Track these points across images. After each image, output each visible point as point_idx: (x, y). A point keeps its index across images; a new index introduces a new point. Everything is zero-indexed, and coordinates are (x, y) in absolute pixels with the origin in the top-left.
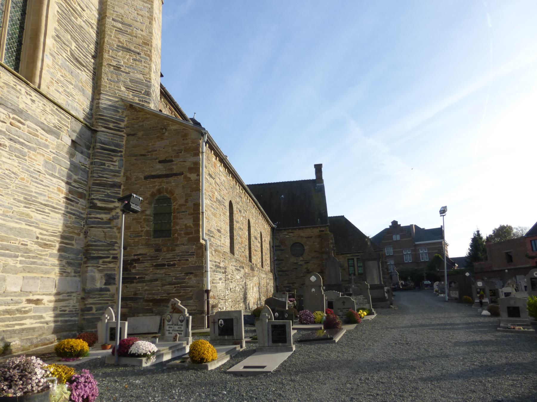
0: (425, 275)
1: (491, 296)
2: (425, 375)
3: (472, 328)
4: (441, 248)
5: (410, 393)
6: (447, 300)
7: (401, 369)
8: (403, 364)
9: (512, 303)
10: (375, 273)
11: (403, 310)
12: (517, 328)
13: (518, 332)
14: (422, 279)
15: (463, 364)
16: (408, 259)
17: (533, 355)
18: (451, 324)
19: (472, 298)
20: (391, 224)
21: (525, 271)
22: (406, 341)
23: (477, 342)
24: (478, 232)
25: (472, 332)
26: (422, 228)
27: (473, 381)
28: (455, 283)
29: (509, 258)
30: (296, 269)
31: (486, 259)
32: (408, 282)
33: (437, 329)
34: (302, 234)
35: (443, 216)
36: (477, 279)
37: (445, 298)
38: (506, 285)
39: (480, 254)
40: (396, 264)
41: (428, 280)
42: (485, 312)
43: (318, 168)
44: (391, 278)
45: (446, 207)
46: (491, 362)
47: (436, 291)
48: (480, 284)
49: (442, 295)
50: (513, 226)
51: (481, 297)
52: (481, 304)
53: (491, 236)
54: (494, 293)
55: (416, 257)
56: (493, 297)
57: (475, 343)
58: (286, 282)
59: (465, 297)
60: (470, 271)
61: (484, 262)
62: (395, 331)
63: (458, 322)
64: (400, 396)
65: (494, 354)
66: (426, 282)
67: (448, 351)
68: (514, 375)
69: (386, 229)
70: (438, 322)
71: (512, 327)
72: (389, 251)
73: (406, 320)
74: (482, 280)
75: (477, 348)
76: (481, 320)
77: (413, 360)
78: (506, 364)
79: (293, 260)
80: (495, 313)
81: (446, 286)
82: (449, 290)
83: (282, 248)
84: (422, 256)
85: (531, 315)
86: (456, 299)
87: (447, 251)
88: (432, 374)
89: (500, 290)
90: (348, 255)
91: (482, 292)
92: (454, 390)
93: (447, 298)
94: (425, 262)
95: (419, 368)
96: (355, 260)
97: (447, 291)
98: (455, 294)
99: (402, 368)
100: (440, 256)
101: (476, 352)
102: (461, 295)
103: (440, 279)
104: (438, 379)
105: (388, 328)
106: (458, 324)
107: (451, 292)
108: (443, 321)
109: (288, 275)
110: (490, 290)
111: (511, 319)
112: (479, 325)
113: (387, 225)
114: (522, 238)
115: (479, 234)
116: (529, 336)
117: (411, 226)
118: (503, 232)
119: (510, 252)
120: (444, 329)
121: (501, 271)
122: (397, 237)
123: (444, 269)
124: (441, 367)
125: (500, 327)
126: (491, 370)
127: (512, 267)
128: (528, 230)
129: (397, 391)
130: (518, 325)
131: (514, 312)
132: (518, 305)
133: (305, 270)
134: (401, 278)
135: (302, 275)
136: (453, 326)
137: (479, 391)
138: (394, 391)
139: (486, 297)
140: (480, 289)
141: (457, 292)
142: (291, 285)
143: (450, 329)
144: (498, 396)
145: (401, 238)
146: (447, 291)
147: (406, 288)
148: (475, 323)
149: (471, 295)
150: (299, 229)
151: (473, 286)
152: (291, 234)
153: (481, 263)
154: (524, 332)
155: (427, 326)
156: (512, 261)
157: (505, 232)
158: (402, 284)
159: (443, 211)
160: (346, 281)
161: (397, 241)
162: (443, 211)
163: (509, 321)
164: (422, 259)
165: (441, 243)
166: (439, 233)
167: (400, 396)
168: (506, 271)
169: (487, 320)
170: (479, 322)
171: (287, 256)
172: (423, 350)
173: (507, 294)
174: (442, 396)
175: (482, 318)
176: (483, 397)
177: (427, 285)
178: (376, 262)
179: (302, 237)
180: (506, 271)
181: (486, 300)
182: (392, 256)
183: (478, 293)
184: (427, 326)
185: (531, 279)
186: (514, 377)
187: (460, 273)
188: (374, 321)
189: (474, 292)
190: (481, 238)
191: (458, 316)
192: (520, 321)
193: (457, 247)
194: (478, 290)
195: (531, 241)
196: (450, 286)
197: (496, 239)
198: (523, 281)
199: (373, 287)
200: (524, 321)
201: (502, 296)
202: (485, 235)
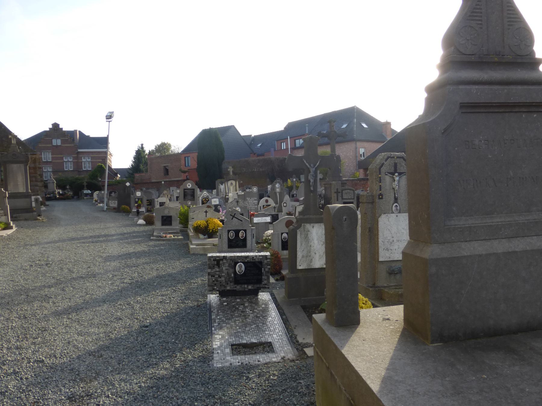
0: (85, 184)
1: (147, 205)
2: (63, 305)
3: (127, 238)
4: (104, 157)
5: (34, 338)
6: (105, 209)
7: (29, 303)
8: (35, 294)
9: (166, 213)
10: (20, 179)
11: (52, 222)
12: (168, 236)
13: (169, 240)
14: (82, 188)
15: (112, 284)
16: (69, 166)
17: (181, 263)
18: (105, 236)
19: (130, 207)
21: (178, 184)
22: (47, 261)
23: (129, 254)
24: (142, 145)
25: (126, 243)
26: (87, 135)
27: (120, 305)
28: (115, 192)
29: (166, 171)
31: (147, 171)
32: (66, 191)
33: (89, 242)
35: (109, 122)
36: (136, 189)
37: (103, 207)
38: (161, 195)
39: (141, 166)
40: (54, 172)
41: (88, 189)
42: (141, 221)
44: (46, 186)
45: (113, 112)
46: (142, 277)
47: (96, 201)
48: (138, 194)
49: (101, 205)
50: (172, 144)
51: (139, 206)
52: (138, 213)
53: (153, 151)
54: (151, 203)
55: (78, 165)
56: (149, 207)
57: (129, 256)
59: (124, 206)
60: (132, 182)
62: (35, 248)
63: (113, 232)
64: (17, 348)
65: (146, 266)
66: (86, 192)
67: (96, 268)
68: (164, 289)
69: (45, 132)
70: (91, 234)
71: (164, 235)
72: (47, 156)
73: (54, 233)
74: (141, 190)
75: (129, 262)
76: (136, 229)
77: (50, 287)
78: (157, 277)
80: (149, 222)
81: (105, 196)
82: (109, 200)
84: (85, 164)
85: (180, 223)
86: (114, 208)
87: (111, 161)
88: (72, 304)
89: (156, 200)
91: (140, 202)
92: (96, 321)
93: (106, 207)
94: (87, 171)
95: (56, 297)
97: (106, 200)
98: (114, 204)
99: (29, 301)
100: (103, 166)
101: (128, 266)
102: (119, 205)
103: (100, 188)
104: (77, 309)
105: (26, 245)
106: (113, 235)
107: (110, 201)
108: (97, 233)
110: (147, 200)
111: (164, 227)
112: (134, 235)
113: (47, 127)
114: (178, 154)
115: (142, 148)
116: (178, 243)
117: (75, 131)
118: (163, 148)
120: (97, 242)
121: (158, 182)
122: (57, 142)
123: (105, 179)
124: (84, 291)
125: (153, 236)
126: (141, 287)
127: (168, 180)
128: (183, 149)
129: (13, 341)
130: (170, 233)
131: (167, 221)
132: (172, 214)
134: (59, 186)
136: (107, 238)
137: (126, 317)
138: (9, 341)
139: (143, 206)
140: (139, 199)
141: (116, 202)
143: (104, 241)
144: (146, 319)
145: (62, 143)
146: (106, 200)
147: (63, 198)
148: (130, 233)
149: (129, 204)
151: (132, 196)
153: (142, 174)
154: (174, 240)
155: (78, 239)
156: (168, 174)
157: (165, 149)
158: (59, 193)
159: (109, 117)
161: (57, 146)
162: (109, 117)
163: (161, 230)
164: (85, 168)
166: (103, 142)
167: (17, 348)
168: (163, 182)
169: (142, 229)
170: (134, 232)
172: (67, 271)
173: (162, 204)
174: (79, 334)
175: (138, 228)
176: (129, 325)
177: (87, 195)
178: (22, 166)
180: (163, 182)
181: (143, 209)
183: (136, 202)
184: (78, 239)
185: (185, 189)
186: (164, 291)
187: (121, 183)
188: (9, 238)
189: (132, 202)
190: (144, 152)
191: (115, 226)
192: (171, 229)
193: (121, 159)
194: (137, 200)
196: (110, 196)
197: (157, 154)
198: (177, 192)
199: (13, 196)
200: (174, 229)
201: (157, 206)
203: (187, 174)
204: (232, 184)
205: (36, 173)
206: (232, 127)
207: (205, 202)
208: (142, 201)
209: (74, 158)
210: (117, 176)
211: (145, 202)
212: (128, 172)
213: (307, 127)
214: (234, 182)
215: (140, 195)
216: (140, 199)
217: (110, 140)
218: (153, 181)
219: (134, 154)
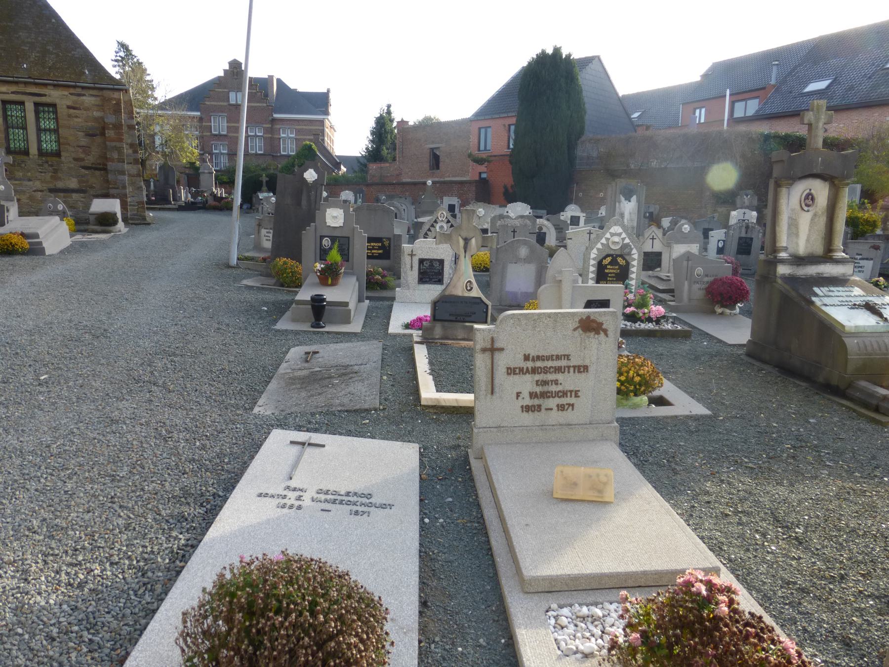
4: (318, 132)
6: (234, 261)
24: (389, 106)
26: (292, 87)
29: (435, 160)
31: (394, 159)
39: (385, 151)
48: (334, 217)
51: (330, 276)
61: (388, 165)
89: (406, 247)
91: (335, 256)
94: (288, 156)
96: (30, 107)
100: (314, 146)
113: (217, 70)
115: (389, 113)
119: (438, 148)
139: (350, 273)
140: (333, 239)
153: (383, 165)
156: (438, 167)
165: (322, 122)
166: (320, 102)
190: (392, 121)
193: (348, 137)
194: (326, 242)
195: (480, 129)
202: (397, 116)
203: (482, 168)
204: (810, 198)
205: (121, 140)
206: (598, 58)
207: (611, 270)
208: (345, 252)
209: (266, 131)
210: (339, 169)
211: (360, 248)
212: (359, 162)
213: (775, 69)
214: (821, 190)
215: (340, 222)
216: (343, 243)
217: (331, 96)
218: (404, 180)
219: (372, 124)
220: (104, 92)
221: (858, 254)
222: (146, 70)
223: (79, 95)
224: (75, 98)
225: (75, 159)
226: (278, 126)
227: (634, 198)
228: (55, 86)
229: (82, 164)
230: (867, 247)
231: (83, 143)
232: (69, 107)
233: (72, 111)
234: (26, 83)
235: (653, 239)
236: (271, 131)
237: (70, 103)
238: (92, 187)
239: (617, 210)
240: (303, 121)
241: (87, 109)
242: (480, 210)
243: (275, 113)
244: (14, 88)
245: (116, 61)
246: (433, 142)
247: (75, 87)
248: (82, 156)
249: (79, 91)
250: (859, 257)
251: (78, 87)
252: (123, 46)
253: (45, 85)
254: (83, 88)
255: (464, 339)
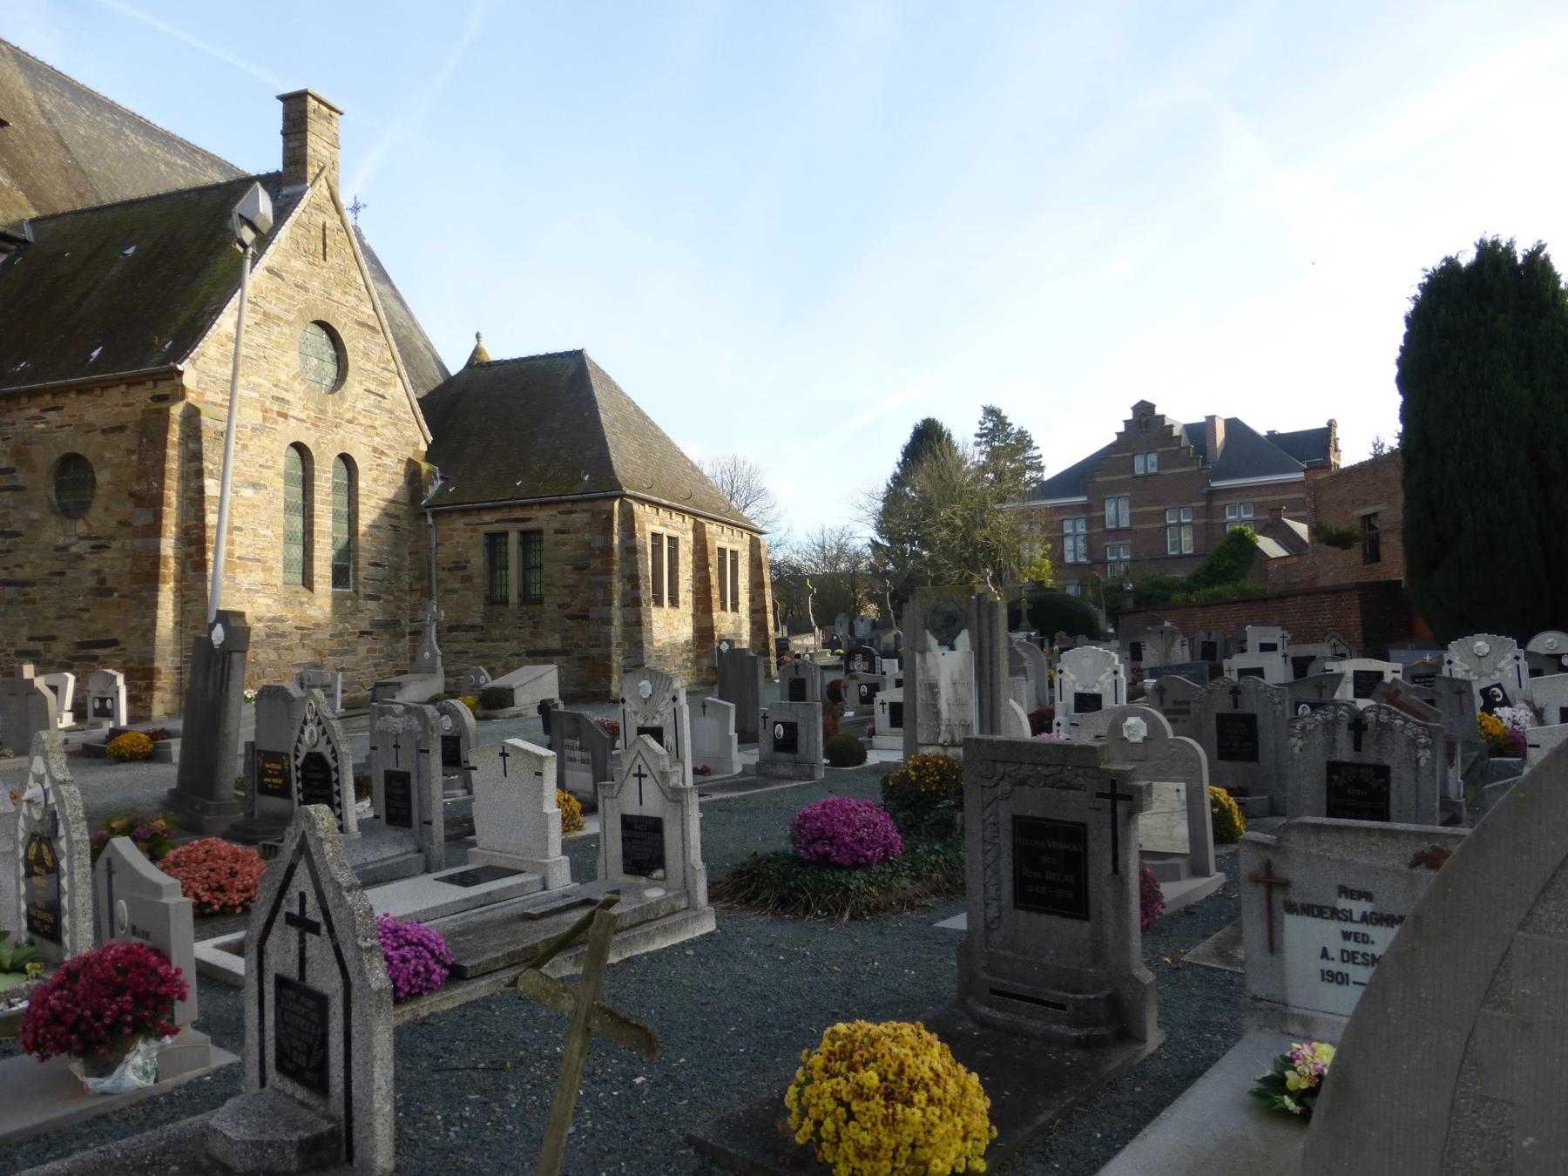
20: (1129, 416)
30: (61, 574)
34: (91, 416)
43: (296, 110)
58: (25, 631)
79: (53, 533)
83: (21, 478)
90: (487, 518)
109: (32, 601)
119: (1375, 515)
122: (1146, 464)
133: (91, 582)
135: (81, 602)
142: (40, 646)
150: (81, 390)
152: (51, 415)
160: (472, 628)
171: (35, 516)
179: (89, 429)
182: (1127, 530)
209: (1197, 513)
217: (1340, 433)
220: (598, 503)
221: (1344, 891)
222: (1031, 442)
223: (570, 512)
224: (564, 517)
225: (560, 606)
226: (1222, 503)
227: (963, 639)
228: (542, 504)
229: (568, 611)
230: (1396, 857)
231: (570, 582)
232: (557, 532)
233: (560, 536)
234: (510, 507)
235: (640, 776)
236: (1208, 511)
237: (557, 526)
238: (577, 646)
239: (920, 676)
240: (1267, 487)
241: (577, 531)
242: (1479, 644)
243: (1214, 480)
244: (498, 515)
245: (981, 436)
246: (1366, 504)
247: (563, 502)
248: (568, 600)
249: (568, 506)
250: (1359, 907)
251: (563, 502)
252: (991, 412)
253: (531, 505)
254: (573, 502)
255: (1213, 969)
